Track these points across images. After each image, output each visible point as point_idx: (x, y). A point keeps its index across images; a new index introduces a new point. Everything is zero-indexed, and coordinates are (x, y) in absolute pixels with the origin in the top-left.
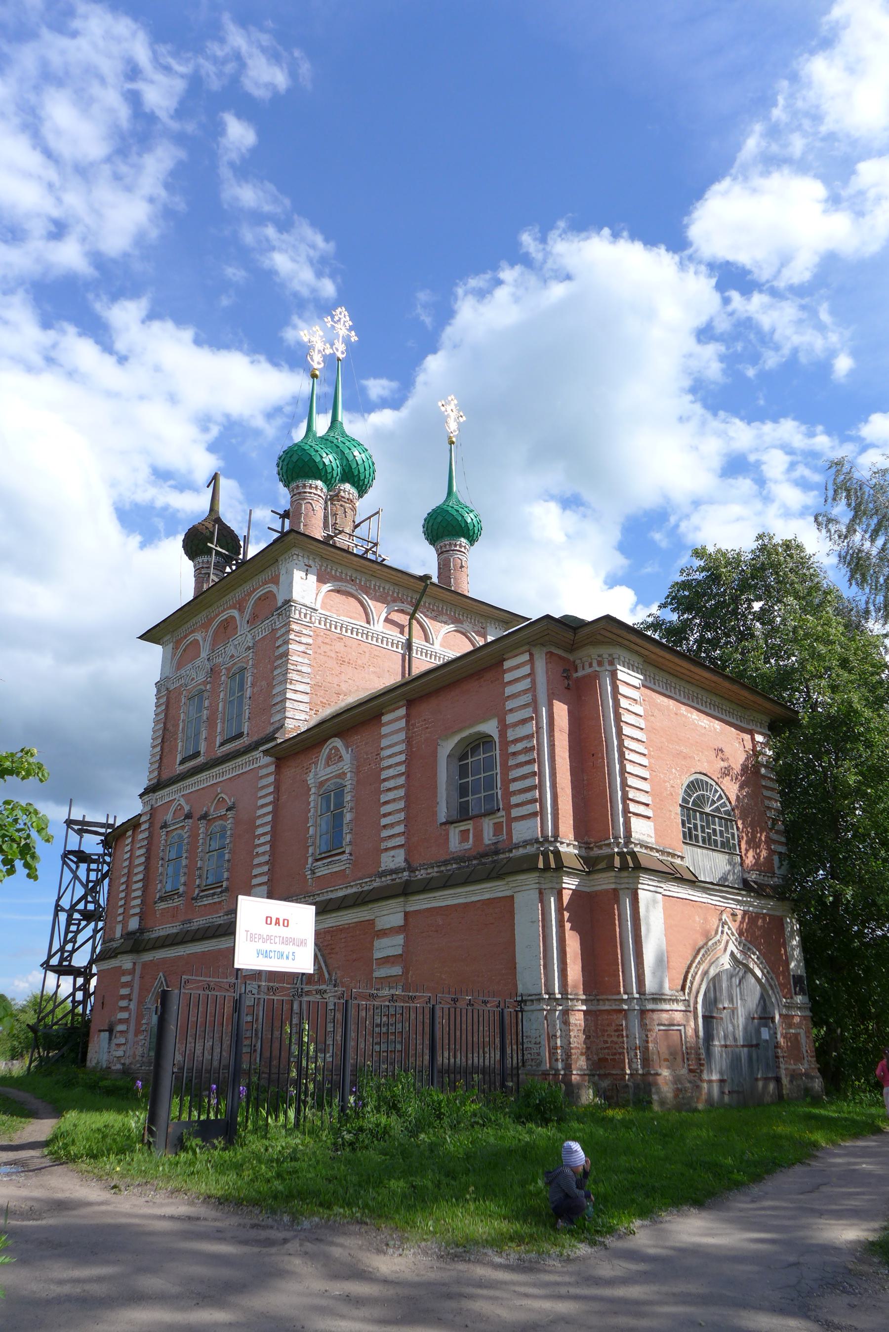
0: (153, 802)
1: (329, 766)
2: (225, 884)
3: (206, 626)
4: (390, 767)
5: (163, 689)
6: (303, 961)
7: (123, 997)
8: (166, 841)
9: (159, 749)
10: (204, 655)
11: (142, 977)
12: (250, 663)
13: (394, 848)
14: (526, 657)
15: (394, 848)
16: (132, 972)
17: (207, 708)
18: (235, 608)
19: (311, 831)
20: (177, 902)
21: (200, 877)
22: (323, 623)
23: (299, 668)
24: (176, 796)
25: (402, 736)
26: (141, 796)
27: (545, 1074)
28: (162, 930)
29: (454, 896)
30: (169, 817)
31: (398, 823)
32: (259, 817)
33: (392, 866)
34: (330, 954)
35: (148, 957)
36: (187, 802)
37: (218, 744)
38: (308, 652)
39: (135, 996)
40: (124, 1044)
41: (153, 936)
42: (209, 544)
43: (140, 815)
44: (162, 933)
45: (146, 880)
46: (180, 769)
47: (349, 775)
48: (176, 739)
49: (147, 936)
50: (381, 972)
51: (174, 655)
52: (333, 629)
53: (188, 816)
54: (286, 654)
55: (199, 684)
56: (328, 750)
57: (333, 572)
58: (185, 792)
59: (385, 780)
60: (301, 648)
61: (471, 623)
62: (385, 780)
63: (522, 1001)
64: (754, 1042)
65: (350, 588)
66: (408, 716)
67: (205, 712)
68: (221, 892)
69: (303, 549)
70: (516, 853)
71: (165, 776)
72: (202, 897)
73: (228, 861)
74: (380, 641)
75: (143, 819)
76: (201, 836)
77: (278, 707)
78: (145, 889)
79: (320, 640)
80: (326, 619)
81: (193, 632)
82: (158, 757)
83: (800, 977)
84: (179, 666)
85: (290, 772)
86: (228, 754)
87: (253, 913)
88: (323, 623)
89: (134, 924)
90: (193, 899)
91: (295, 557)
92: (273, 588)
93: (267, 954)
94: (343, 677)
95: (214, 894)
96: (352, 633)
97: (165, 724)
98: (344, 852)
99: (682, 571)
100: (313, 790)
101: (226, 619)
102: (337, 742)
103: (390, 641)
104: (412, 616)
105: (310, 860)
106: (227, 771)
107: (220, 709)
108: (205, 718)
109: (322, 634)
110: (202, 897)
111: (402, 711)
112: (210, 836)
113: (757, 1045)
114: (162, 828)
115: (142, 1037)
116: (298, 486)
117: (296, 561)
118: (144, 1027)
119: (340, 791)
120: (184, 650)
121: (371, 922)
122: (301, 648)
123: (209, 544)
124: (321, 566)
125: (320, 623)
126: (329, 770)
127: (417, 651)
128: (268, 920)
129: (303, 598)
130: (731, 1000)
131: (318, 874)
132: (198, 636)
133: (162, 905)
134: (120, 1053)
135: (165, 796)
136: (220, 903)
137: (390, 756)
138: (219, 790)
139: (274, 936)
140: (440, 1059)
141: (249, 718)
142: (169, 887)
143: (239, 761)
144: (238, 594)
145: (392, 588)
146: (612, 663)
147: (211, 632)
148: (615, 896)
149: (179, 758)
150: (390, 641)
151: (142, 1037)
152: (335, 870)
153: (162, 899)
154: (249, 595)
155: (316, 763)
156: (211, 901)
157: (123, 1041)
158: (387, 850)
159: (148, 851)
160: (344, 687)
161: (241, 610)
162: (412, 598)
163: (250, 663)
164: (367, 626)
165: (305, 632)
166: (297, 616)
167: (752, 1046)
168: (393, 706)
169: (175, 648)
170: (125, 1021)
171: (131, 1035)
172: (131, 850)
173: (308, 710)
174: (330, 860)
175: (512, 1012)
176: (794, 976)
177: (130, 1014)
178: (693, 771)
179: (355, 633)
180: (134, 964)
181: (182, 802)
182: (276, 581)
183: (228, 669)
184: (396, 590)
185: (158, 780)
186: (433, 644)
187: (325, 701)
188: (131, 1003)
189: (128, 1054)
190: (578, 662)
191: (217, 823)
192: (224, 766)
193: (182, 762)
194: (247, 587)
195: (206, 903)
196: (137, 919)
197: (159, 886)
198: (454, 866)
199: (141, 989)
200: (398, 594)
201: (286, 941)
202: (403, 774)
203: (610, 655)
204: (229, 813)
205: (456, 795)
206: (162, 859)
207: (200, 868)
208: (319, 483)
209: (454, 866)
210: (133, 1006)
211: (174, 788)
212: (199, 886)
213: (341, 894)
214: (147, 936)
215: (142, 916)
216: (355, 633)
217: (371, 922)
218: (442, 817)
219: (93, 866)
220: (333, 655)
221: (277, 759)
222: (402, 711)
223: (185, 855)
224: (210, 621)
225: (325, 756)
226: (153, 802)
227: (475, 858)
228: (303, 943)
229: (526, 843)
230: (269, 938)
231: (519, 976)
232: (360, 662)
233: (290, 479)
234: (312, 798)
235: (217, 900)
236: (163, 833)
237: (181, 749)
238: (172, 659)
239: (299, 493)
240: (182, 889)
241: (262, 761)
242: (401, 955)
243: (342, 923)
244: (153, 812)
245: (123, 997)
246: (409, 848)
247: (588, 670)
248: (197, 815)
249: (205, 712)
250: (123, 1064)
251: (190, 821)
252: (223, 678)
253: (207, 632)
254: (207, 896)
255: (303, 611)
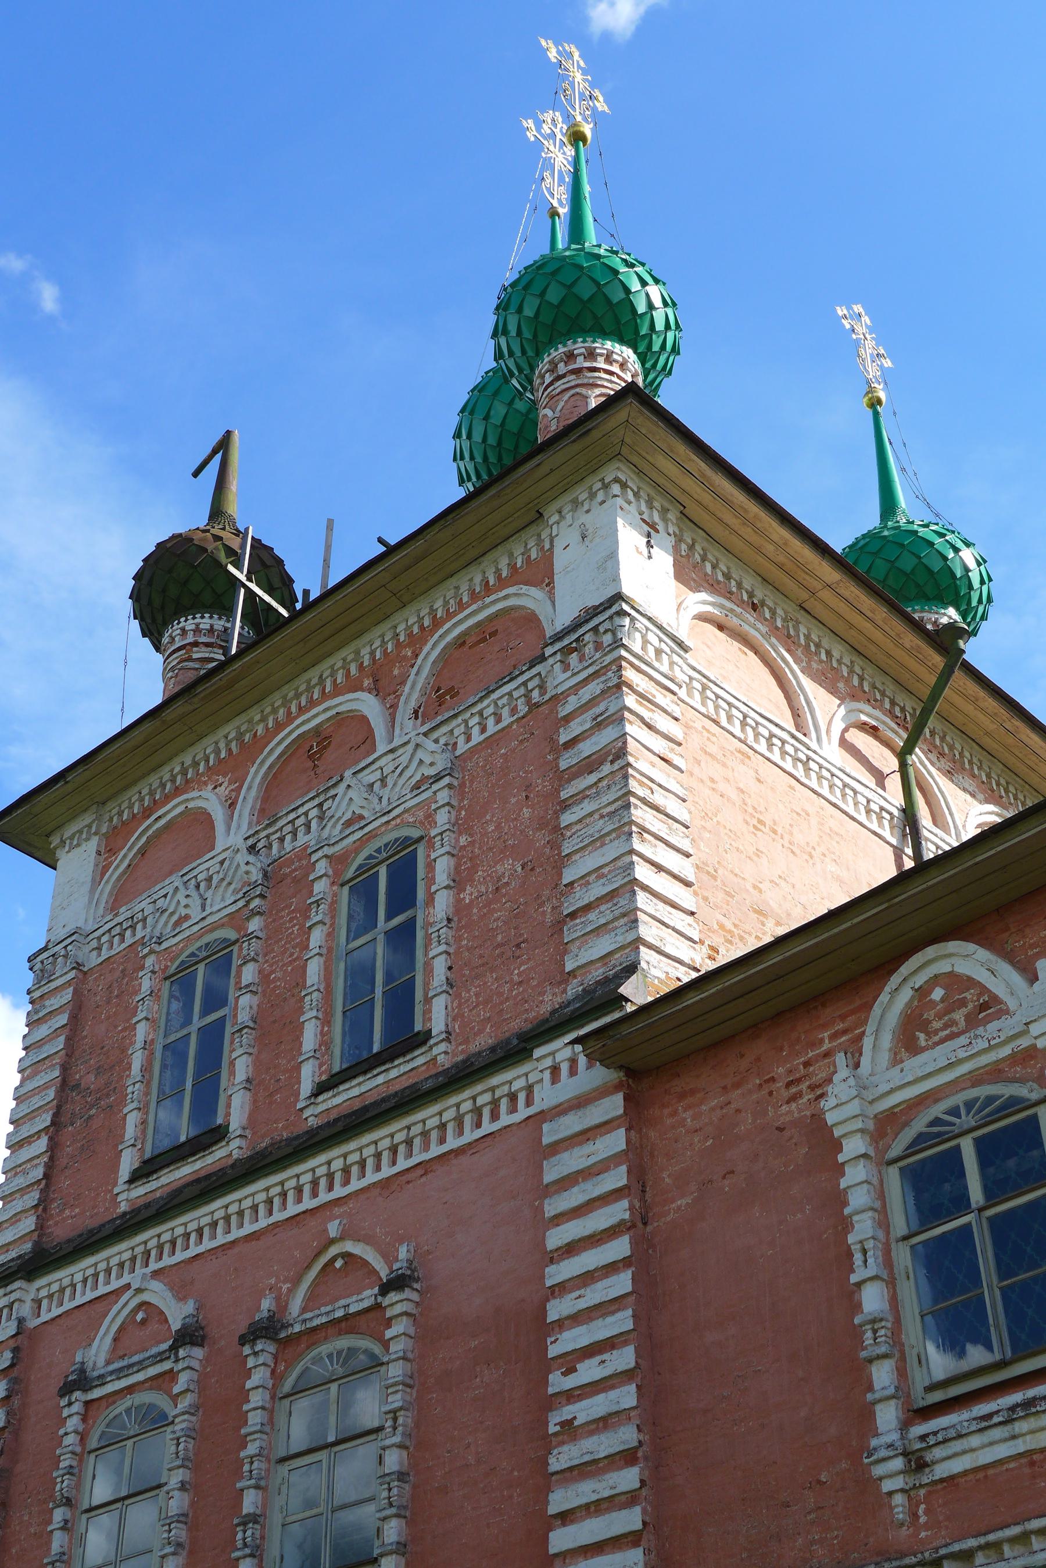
0: (25, 1310)
8: (83, 1437)
9: (42, 1144)
12: (442, 818)
24: (134, 1279)
30: (97, 1353)
36: (181, 1293)
37: (306, 1087)
48: (122, 1101)
51: (102, 871)
53: (190, 1335)
56: (906, 995)
58: (167, 1261)
65: (755, 629)
67: (245, 1000)
69: (640, 472)
71: (66, 1226)
76: (257, 1399)
80: (705, 688)
82: (39, 1173)
84: (119, 898)
91: (616, 489)
97: (65, 1068)
104: (903, 755)
105: (887, 1416)
114: (67, 1389)
116: (571, 356)
117: (619, 501)
120: (143, 852)
131: (941, 1471)
132: (209, 800)
137: (577, 1318)
138: (333, 1229)
143: (428, 1115)
144: (371, 646)
145: (846, 660)
147: (256, 775)
149: (128, 1162)
154: (416, 641)
163: (442, 818)
169: (109, 849)
174: (1017, 1397)
181: (158, 1294)
183: (338, 861)
185: (37, 1244)
187: (729, 925)
191: (324, 1349)
192: (352, 1145)
194: (407, 621)
204: (393, 1297)
206: (68, 1502)
207: (253, 1519)
211: (119, 1251)
221: (631, 1072)
225: (893, 1017)
226: (25, 1310)
234: (855, 1174)
236: (73, 1410)
238: (96, 882)
239: (577, 372)
241: (561, 1078)
249: (245, 1000)
251: (198, 1352)
252: (320, 887)
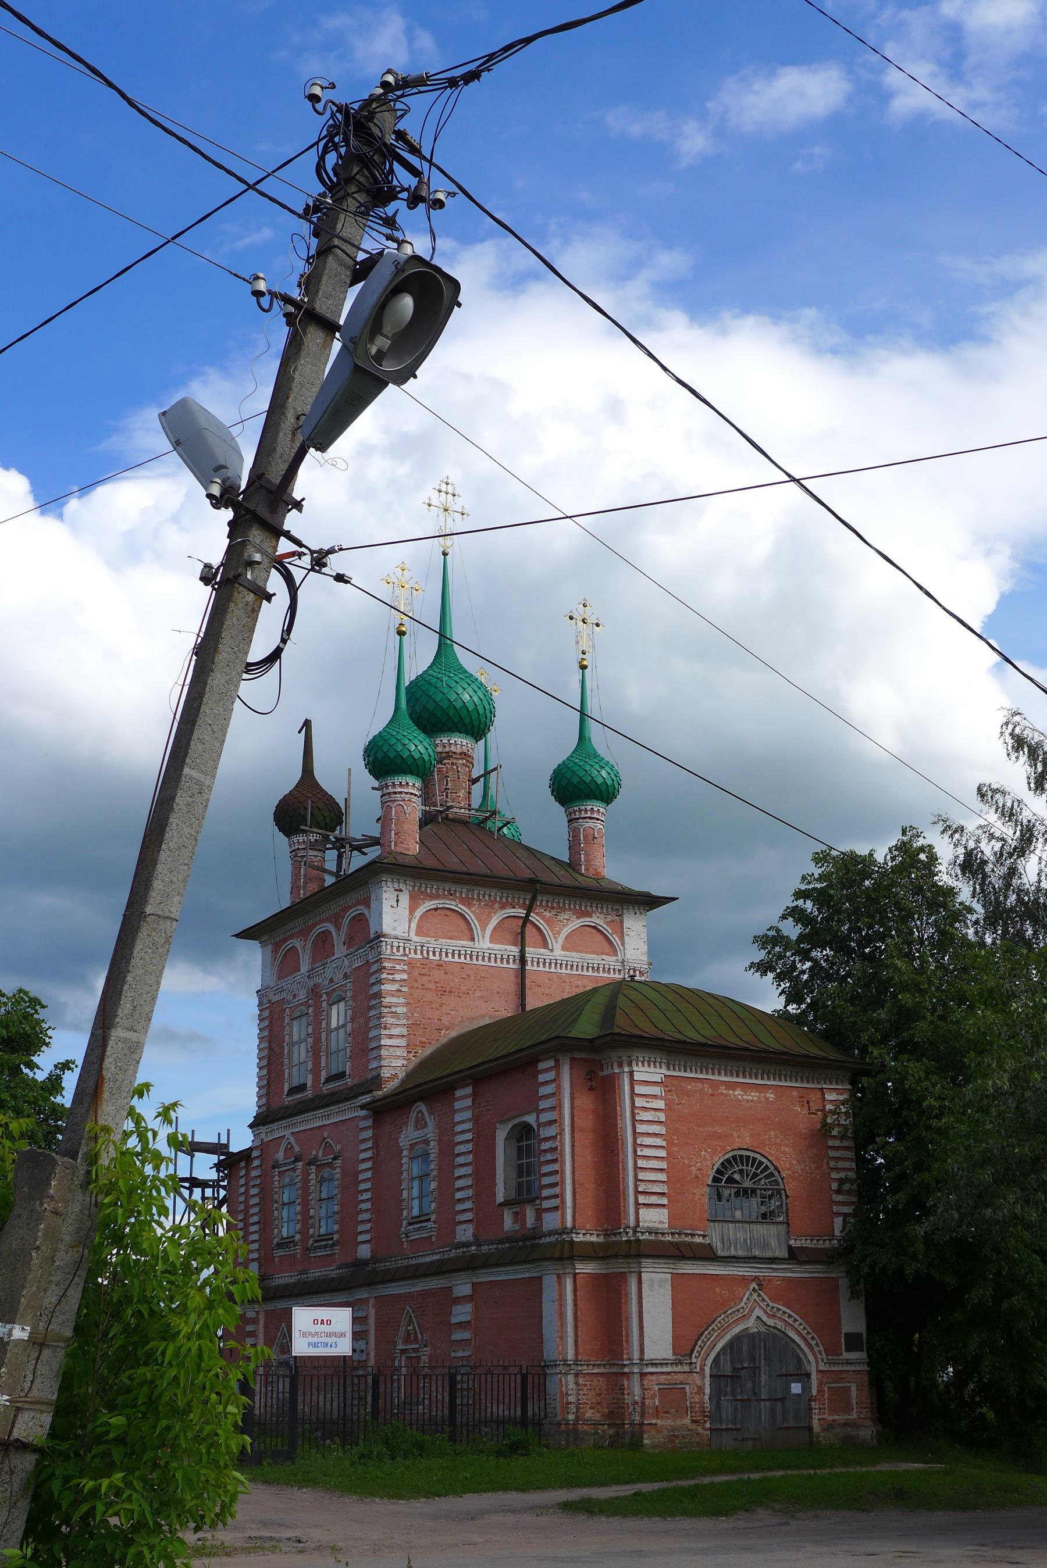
2: (336, 1237)
4: (461, 1143)
6: (344, 1347)
10: (304, 969)
11: (266, 1327)
13: (466, 1222)
14: (551, 1063)
15: (466, 1222)
22: (419, 952)
23: (393, 1009)
26: (251, 1126)
27: (559, 1424)
29: (507, 1273)
30: (280, 1156)
31: (468, 1198)
33: (464, 1239)
36: (297, 1141)
43: (250, 1149)
44: (281, 1282)
46: (288, 1100)
50: (457, 1336)
52: (431, 957)
54: (378, 995)
55: (301, 1004)
57: (428, 891)
59: (458, 1155)
60: (394, 987)
61: (601, 913)
62: (458, 1155)
63: (545, 1366)
64: (779, 1396)
66: (474, 1095)
70: (543, 1241)
72: (316, 1248)
74: (486, 959)
77: (374, 1054)
78: (262, 1232)
79: (416, 972)
81: (291, 937)
83: (858, 1335)
84: (281, 975)
87: (303, 1317)
88: (419, 952)
92: (362, 909)
93: (315, 1345)
94: (444, 1009)
96: (453, 957)
98: (429, 1220)
99: (804, 878)
100: (405, 1153)
102: (422, 1107)
103: (499, 956)
105: (404, 1223)
107: (323, 1040)
110: (316, 1248)
111: (469, 1090)
112: (322, 1181)
113: (782, 1399)
114: (274, 1167)
122: (394, 987)
124: (414, 887)
125: (416, 953)
127: (532, 962)
128: (315, 1322)
129: (395, 929)
130: (752, 1359)
139: (322, 1330)
140: (300, 1407)
146: (630, 1064)
148: (623, 1277)
150: (499, 956)
153: (279, 1245)
155: (406, 1123)
158: (461, 1223)
160: (446, 1020)
161: (338, 927)
162: (525, 899)
164: (471, 943)
165: (398, 967)
167: (776, 1400)
173: (405, 1054)
175: (534, 1377)
176: (846, 1334)
178: (729, 1148)
179: (456, 956)
181: (292, 1140)
182: (367, 903)
184: (505, 895)
186: (552, 950)
190: (603, 1062)
194: (342, 902)
197: (276, 1231)
198: (507, 1245)
200: (507, 898)
201: (329, 1335)
202: (470, 1152)
203: (629, 1057)
205: (513, 1175)
208: (411, 780)
209: (507, 1245)
213: (428, 1259)
216: (456, 956)
218: (500, 1198)
219: (209, 1192)
220: (432, 986)
221: (374, 1112)
222: (469, 1090)
226: (263, 1136)
227: (520, 1240)
228: (343, 1335)
229: (551, 1233)
230: (316, 1334)
231: (545, 1346)
232: (463, 988)
234: (404, 1160)
238: (272, 965)
242: (470, 1322)
246: (478, 1224)
247: (610, 1072)
253: (305, 941)
254: (320, 1247)
255: (396, 944)
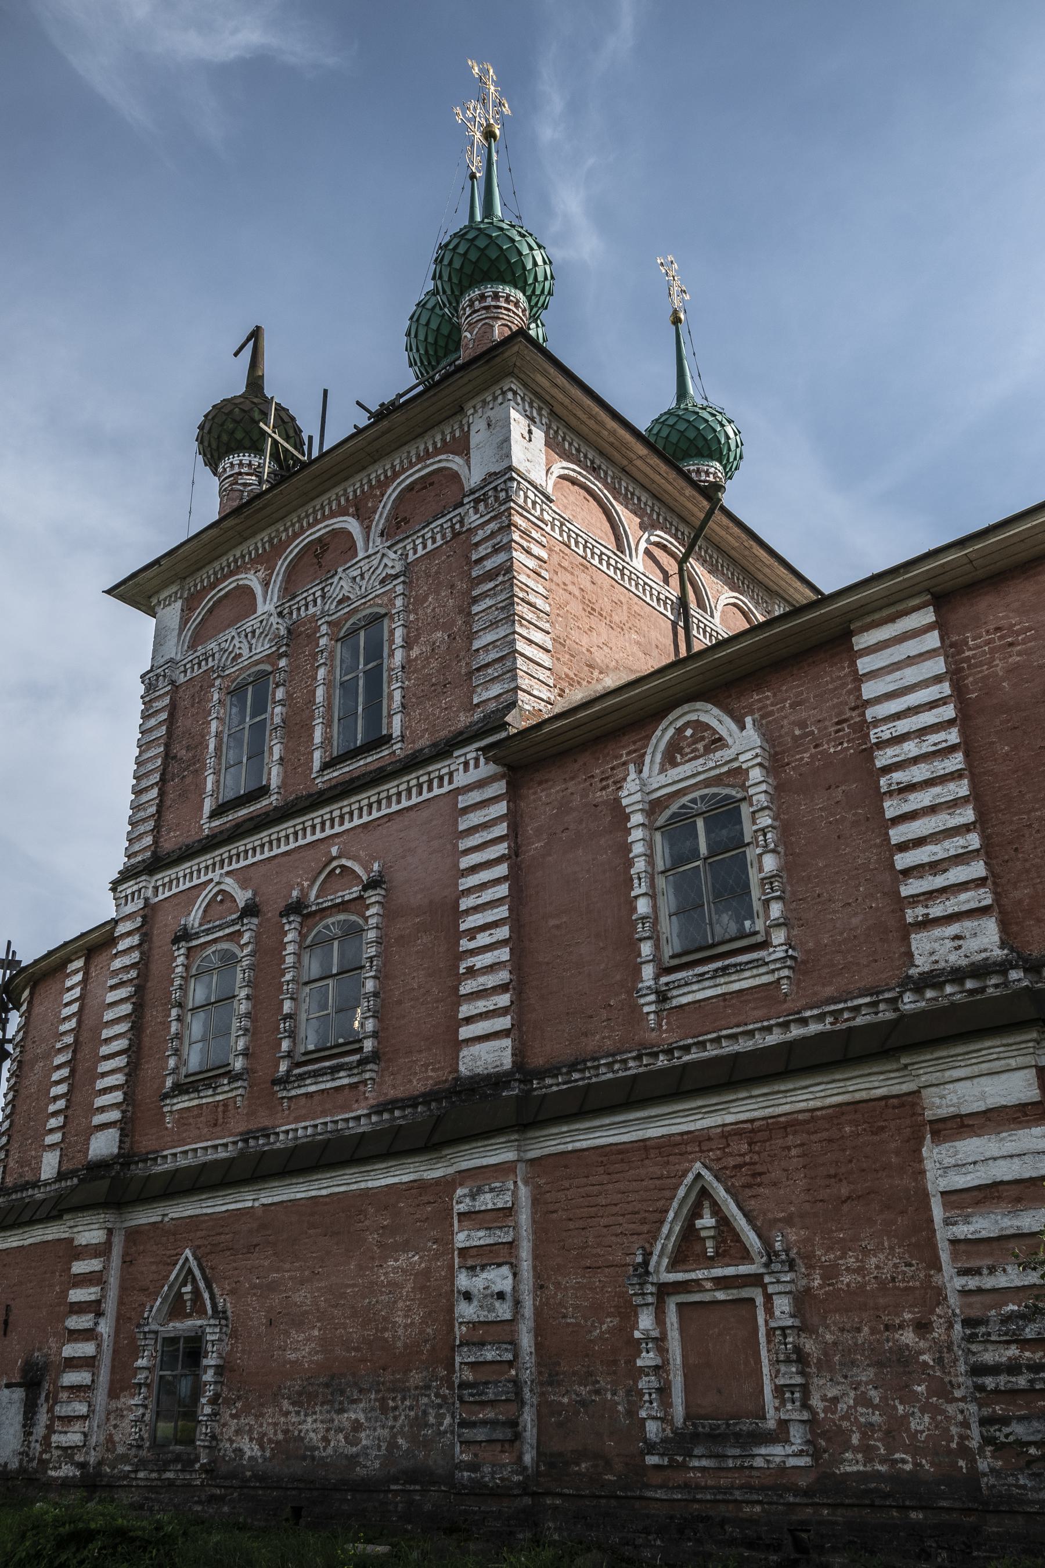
0: (150, 893)
1: (674, 764)
2: (368, 1045)
3: (266, 560)
5: (164, 687)
7: (79, 1308)
8: (187, 967)
16: (102, 1251)
17: (282, 703)
18: (345, 513)
19: (643, 907)
20: (226, 1092)
21: (292, 1035)
24: (215, 876)
25: (938, 666)
28: (180, 1156)
30: (194, 918)
32: (468, 892)
34: (749, 1186)
35: (145, 1217)
37: (317, 765)
38: (544, 573)
39: (110, 1306)
40: (84, 1418)
41: (159, 1169)
42: (262, 425)
45: (135, 1053)
47: (756, 774)
49: (139, 1170)
53: (251, 910)
56: (671, 732)
58: (235, 866)
68: (361, 1063)
71: (170, 843)
72: (301, 1077)
73: (376, 994)
75: (122, 928)
76: (290, 948)
78: (132, 1070)
80: (562, 524)
85: (544, 798)
86: (352, 780)
89: (103, 1145)
90: (276, 1082)
92: (455, 463)
95: (335, 1070)
97: (167, 746)
100: (637, 818)
101: (320, 539)
105: (648, 972)
106: (359, 812)
108: (277, 720)
109: (557, 549)
114: (176, 940)
115: (137, 1400)
116: (483, 297)
118: (141, 1377)
119: (725, 814)
120: (211, 611)
121: (910, 1102)
123: (262, 425)
126: (674, 773)
131: (675, 1003)
132: (252, 580)
133: (183, 1102)
134: (73, 1438)
135: (179, 879)
136: (353, 1086)
138: (334, 851)
141: (403, 706)
142: (194, 1060)
143: (391, 787)
147: (281, 566)
149: (208, 806)
151: (137, 1400)
152: (736, 987)
153: (180, 1089)
156: (329, 1085)
157: (82, 1409)
159: (140, 990)
160: (599, 656)
161: (363, 515)
163: (399, 602)
165: (534, 534)
166: (521, 501)
168: (885, 613)
169: (188, 608)
170: (88, 1363)
171: (100, 1397)
172: (81, 998)
174: (719, 964)
177: (99, 1346)
180: (110, 1232)
185: (154, 853)
188: (102, 1321)
189: (93, 1440)
193: (214, 815)
195: (312, 1089)
196: (113, 1133)
197: (172, 1062)
199: (124, 1289)
204: (370, 892)
206: (180, 1005)
207: (289, 1016)
210: (105, 1328)
212: (289, 1054)
214: (139, 1170)
215: (126, 1127)
217: (910, 1102)
223: (243, 993)
224: (278, 549)
233: (465, 283)
235: (346, 1081)
237: (213, 785)
238: (181, 630)
240: (239, 1064)
241: (469, 770)
243: (787, 1108)
244: (149, 913)
245: (79, 1308)
248: (272, 909)
249: (278, 710)
250: (82, 1466)
251: (255, 921)
252: (323, 641)
254: (316, 1074)
